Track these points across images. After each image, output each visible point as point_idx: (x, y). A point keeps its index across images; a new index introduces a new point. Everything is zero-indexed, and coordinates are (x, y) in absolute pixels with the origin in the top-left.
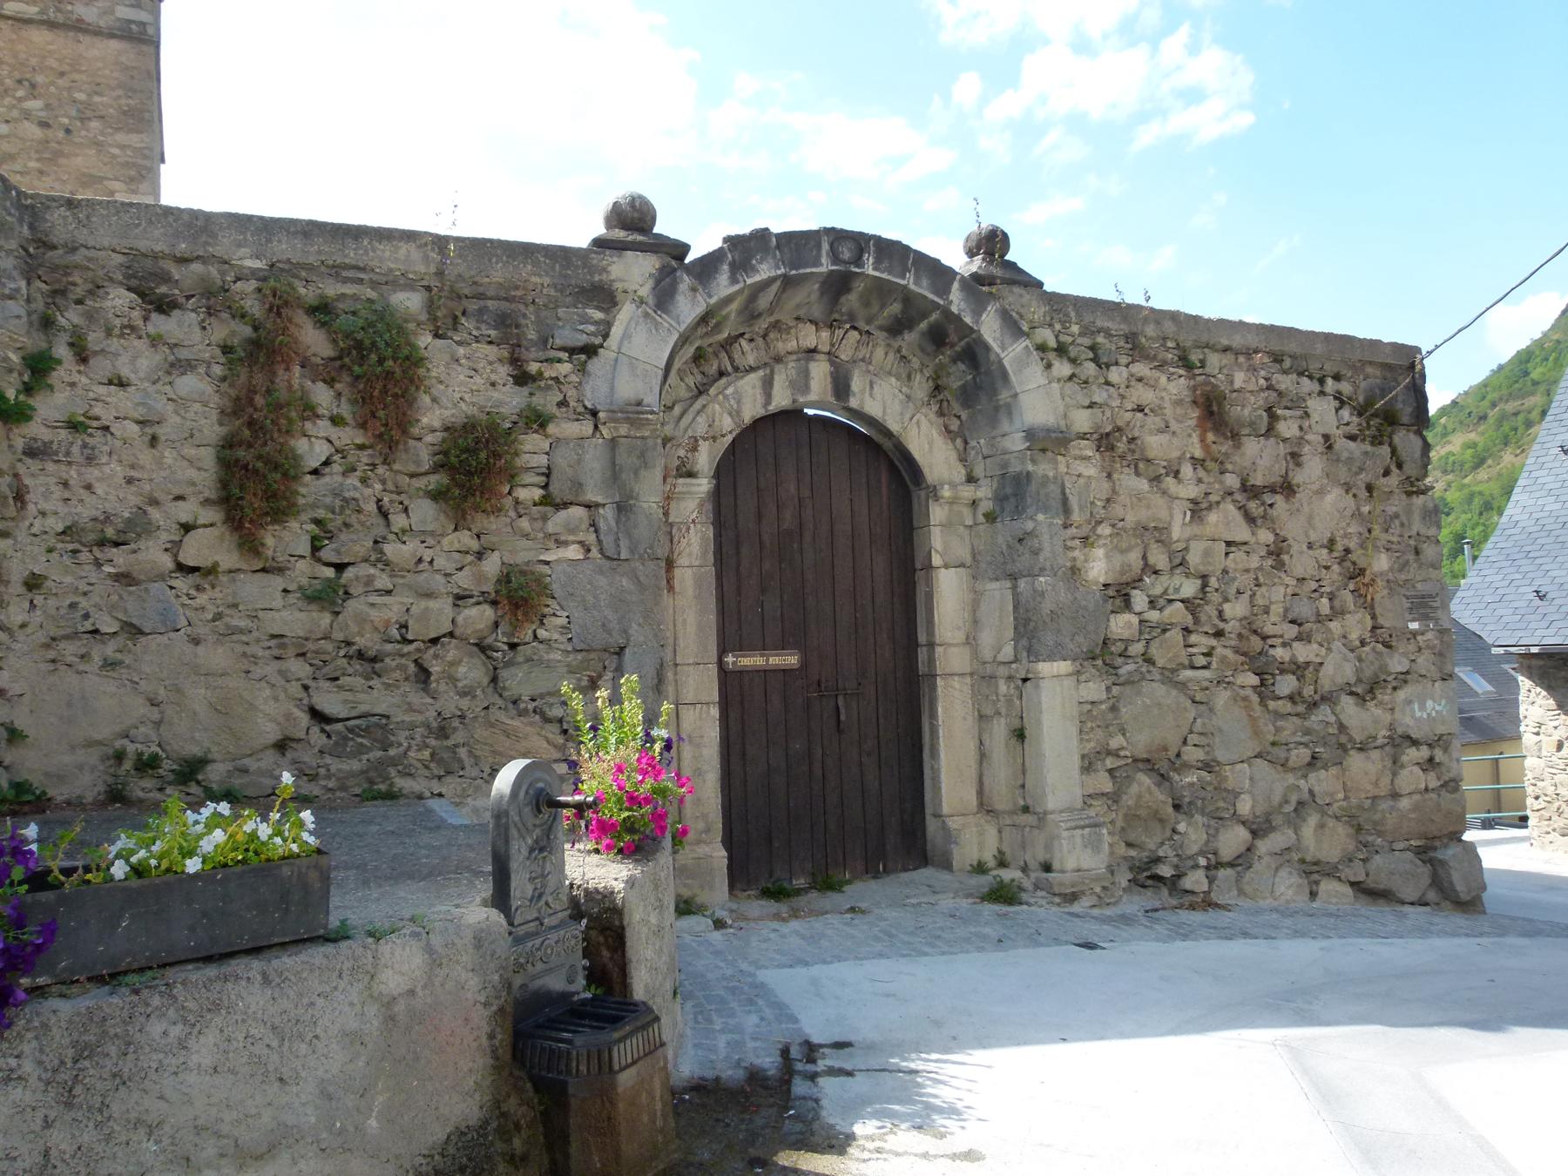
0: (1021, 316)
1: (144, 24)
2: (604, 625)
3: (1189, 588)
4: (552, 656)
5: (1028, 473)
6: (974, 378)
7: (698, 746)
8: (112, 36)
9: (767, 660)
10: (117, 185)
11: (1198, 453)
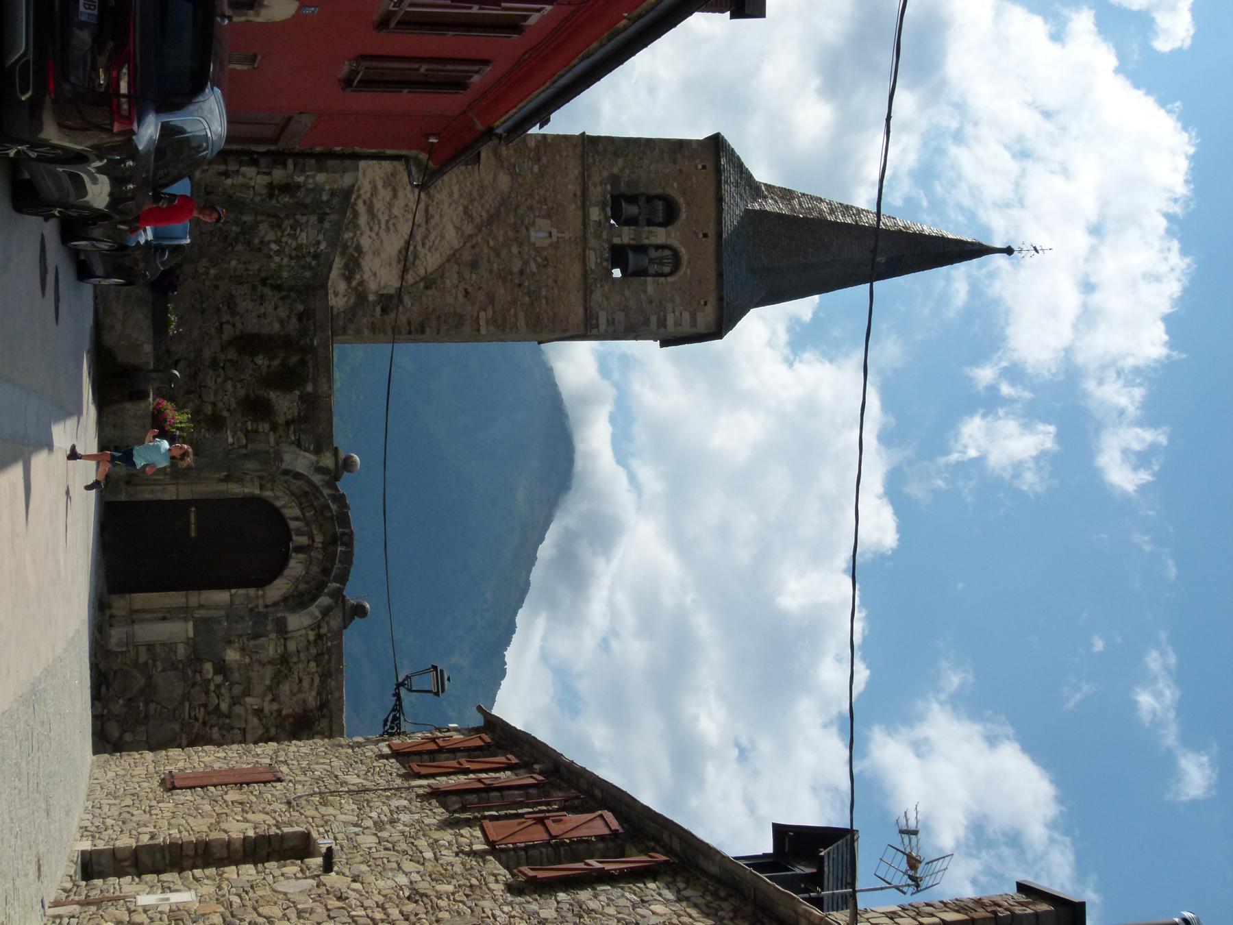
1: (597, 326)
3: (224, 707)
8: (586, 309)
10: (490, 312)
11: (284, 712)
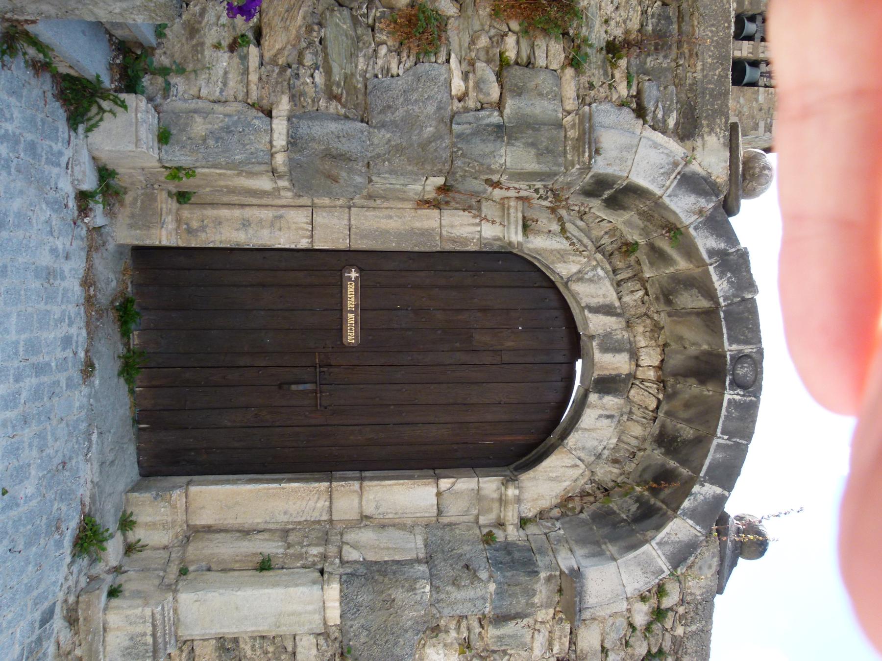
0: (690, 567)
2: (389, 107)
4: (361, 60)
5: (537, 573)
6: (624, 520)
7: (272, 225)
9: (351, 312)
